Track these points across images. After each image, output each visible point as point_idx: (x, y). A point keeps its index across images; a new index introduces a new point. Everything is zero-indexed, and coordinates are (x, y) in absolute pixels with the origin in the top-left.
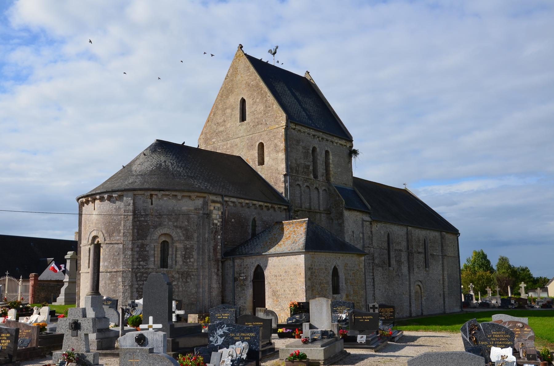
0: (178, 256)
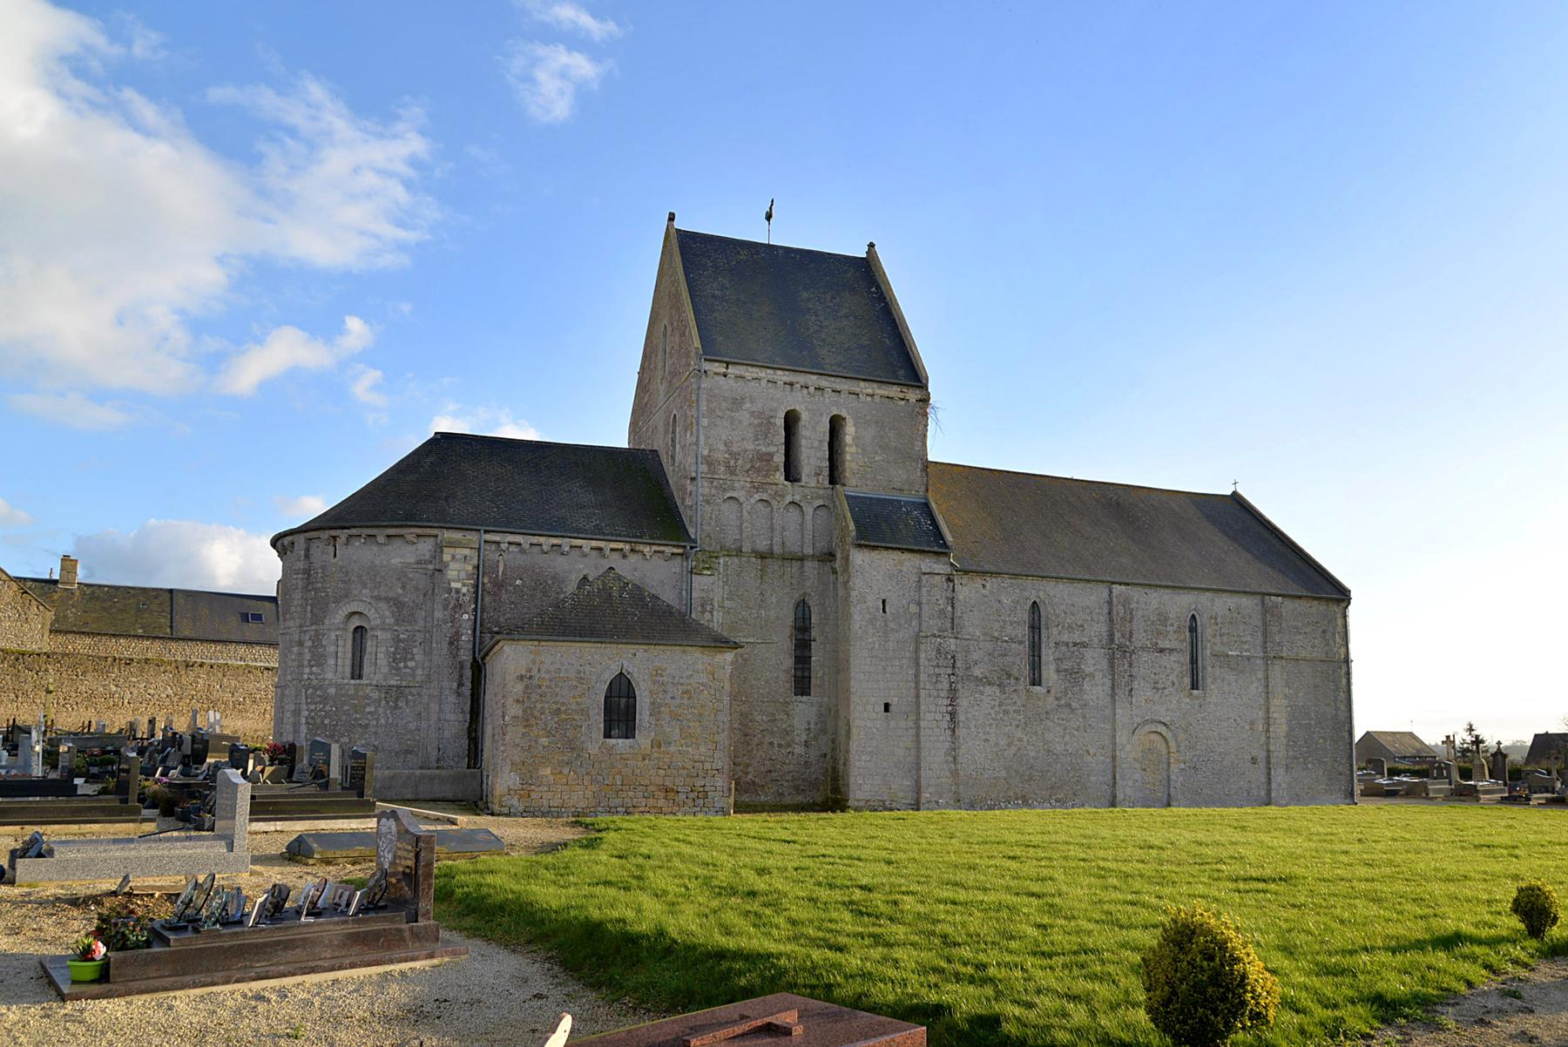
0: (380, 656)
